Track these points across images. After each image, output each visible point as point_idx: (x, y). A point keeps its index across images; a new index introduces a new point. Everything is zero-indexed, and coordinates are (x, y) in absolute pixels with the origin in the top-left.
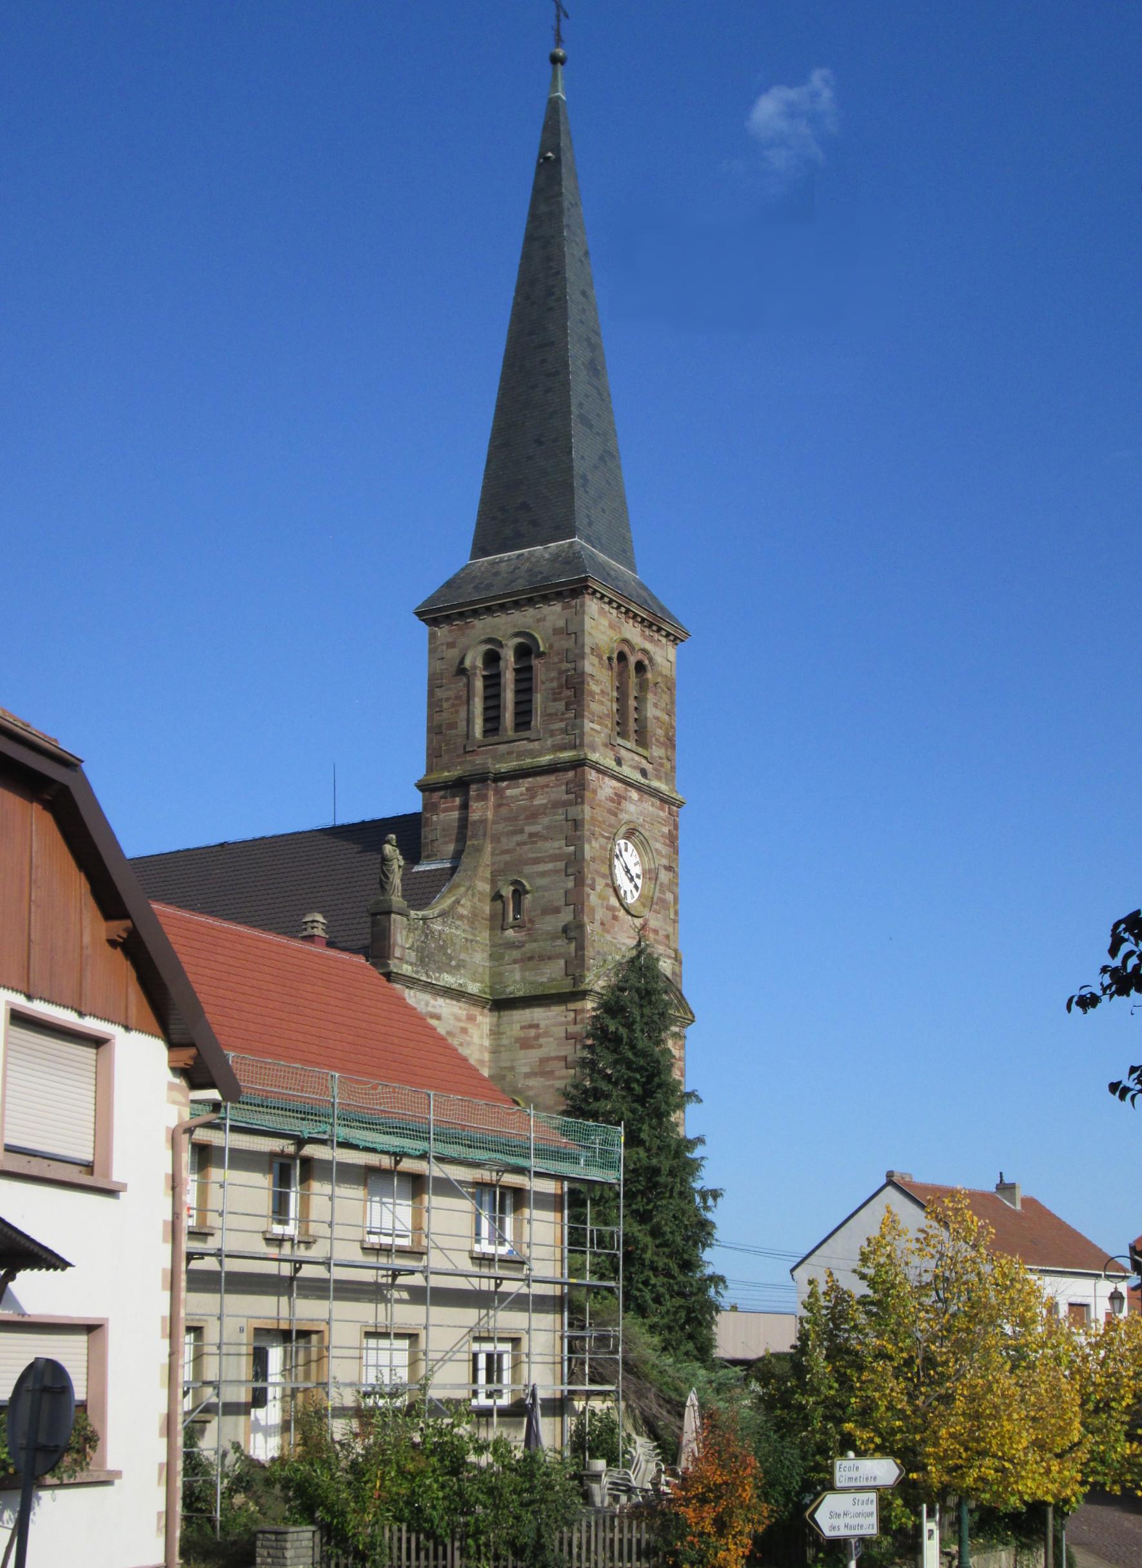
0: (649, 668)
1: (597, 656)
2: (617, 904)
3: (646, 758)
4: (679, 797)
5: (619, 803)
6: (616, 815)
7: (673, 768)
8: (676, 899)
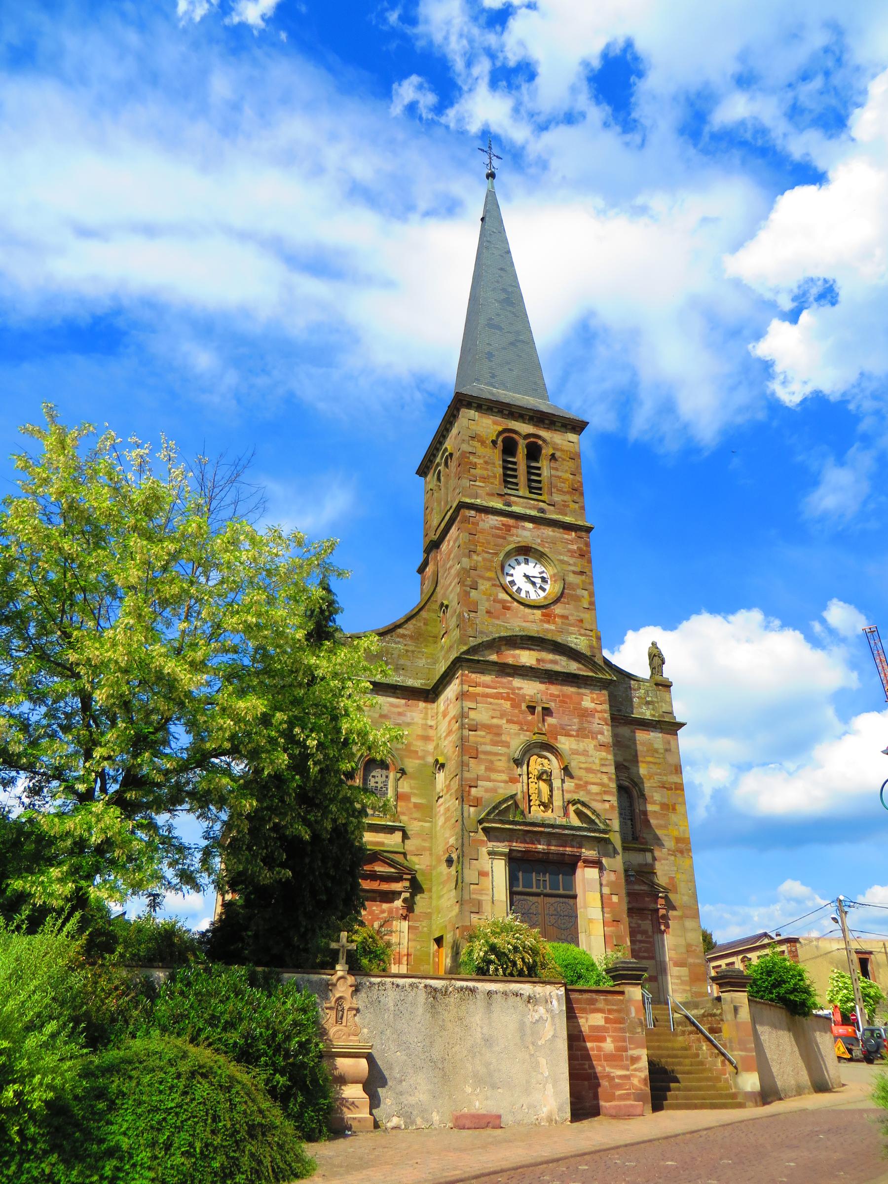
0: (544, 445)
1: (478, 441)
2: (509, 599)
3: (544, 502)
4: (588, 524)
5: (509, 531)
6: (504, 538)
7: (583, 508)
8: (592, 595)
